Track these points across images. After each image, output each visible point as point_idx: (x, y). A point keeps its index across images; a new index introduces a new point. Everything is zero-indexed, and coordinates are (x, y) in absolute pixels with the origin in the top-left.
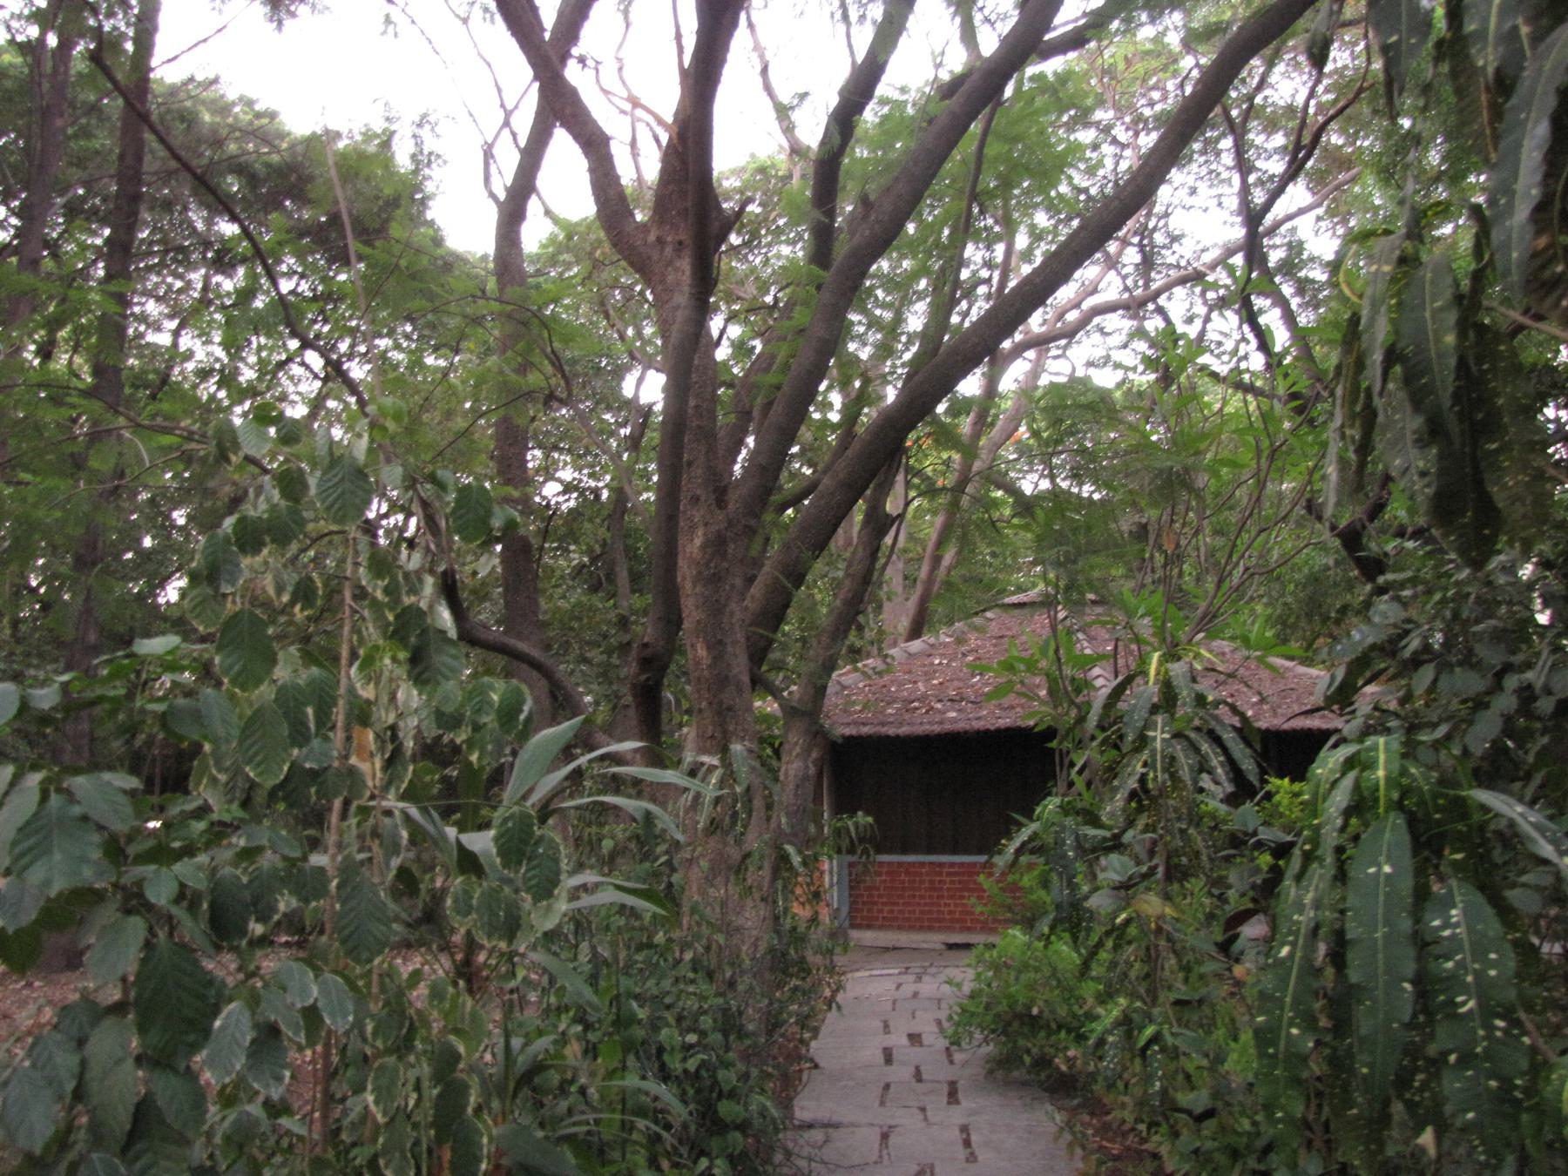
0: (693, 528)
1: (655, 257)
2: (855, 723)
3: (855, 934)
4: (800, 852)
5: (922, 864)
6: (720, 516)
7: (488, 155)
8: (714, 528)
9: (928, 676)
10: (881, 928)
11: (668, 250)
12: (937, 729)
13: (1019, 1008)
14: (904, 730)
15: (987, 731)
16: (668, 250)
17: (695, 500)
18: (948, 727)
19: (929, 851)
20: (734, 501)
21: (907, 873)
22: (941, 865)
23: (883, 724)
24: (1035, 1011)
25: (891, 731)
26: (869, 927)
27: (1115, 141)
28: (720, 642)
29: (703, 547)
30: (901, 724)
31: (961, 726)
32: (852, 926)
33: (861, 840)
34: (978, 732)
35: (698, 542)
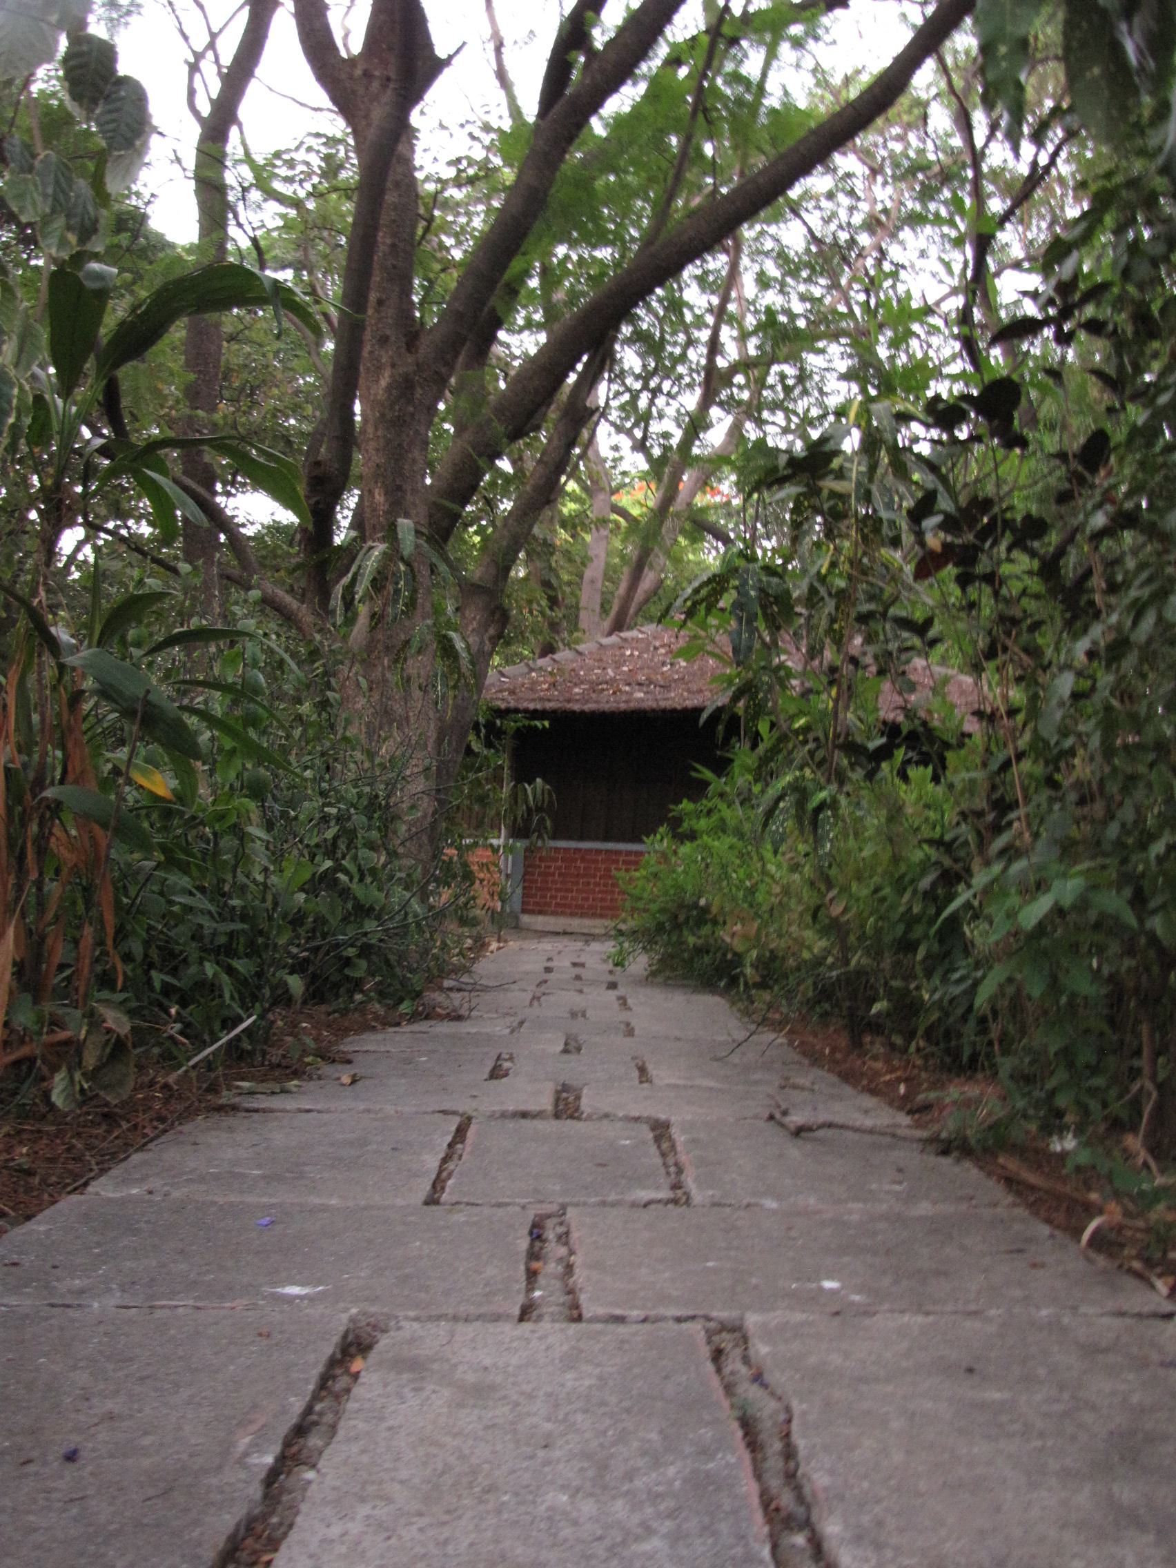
0: (379, 368)
1: (361, 91)
2: (541, 699)
3: (526, 919)
4: (464, 639)
5: (598, 852)
6: (410, 359)
7: (194, 68)
8: (401, 370)
9: (617, 665)
10: (554, 914)
11: (376, 85)
12: (623, 706)
13: (688, 899)
14: (588, 707)
15: (674, 711)
16: (376, 85)
17: (384, 340)
18: (633, 705)
19: (606, 838)
20: (425, 347)
21: (583, 860)
22: (618, 853)
23: (569, 701)
24: (702, 902)
25: (576, 707)
26: (540, 913)
27: (851, 193)
28: (399, 488)
29: (389, 388)
30: (587, 702)
31: (650, 704)
32: (524, 911)
33: (539, 809)
34: (664, 711)
35: (384, 383)
